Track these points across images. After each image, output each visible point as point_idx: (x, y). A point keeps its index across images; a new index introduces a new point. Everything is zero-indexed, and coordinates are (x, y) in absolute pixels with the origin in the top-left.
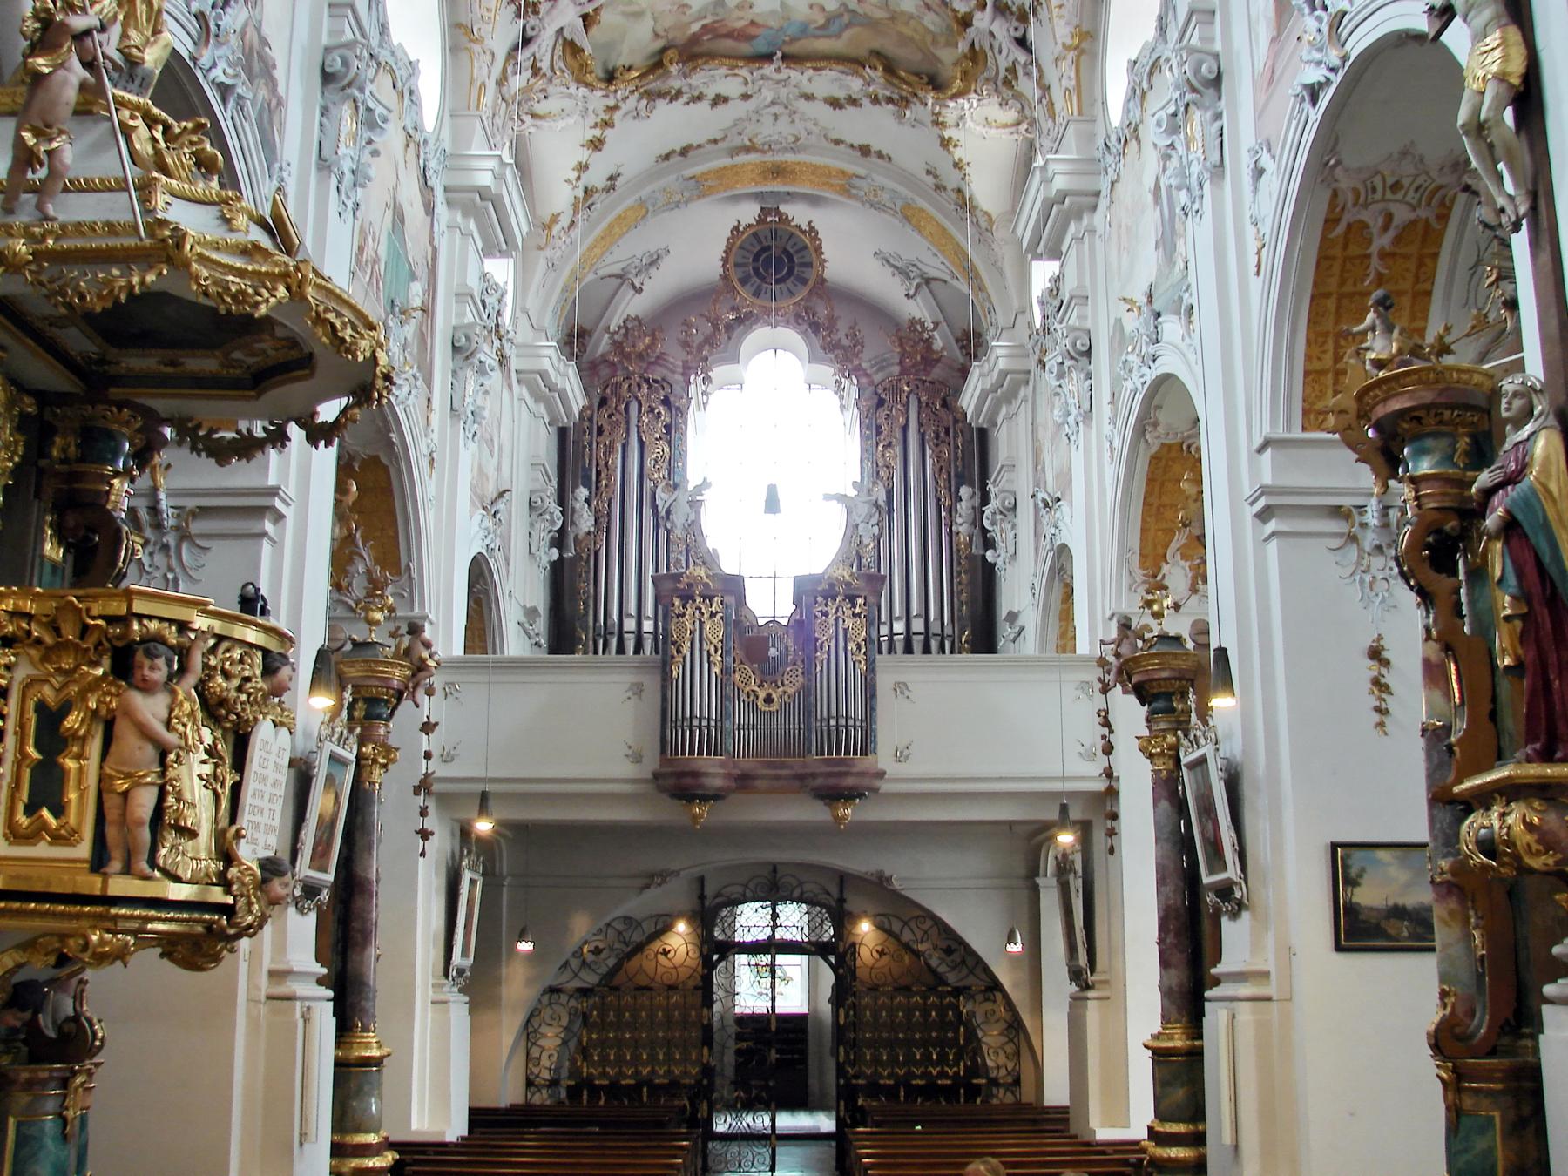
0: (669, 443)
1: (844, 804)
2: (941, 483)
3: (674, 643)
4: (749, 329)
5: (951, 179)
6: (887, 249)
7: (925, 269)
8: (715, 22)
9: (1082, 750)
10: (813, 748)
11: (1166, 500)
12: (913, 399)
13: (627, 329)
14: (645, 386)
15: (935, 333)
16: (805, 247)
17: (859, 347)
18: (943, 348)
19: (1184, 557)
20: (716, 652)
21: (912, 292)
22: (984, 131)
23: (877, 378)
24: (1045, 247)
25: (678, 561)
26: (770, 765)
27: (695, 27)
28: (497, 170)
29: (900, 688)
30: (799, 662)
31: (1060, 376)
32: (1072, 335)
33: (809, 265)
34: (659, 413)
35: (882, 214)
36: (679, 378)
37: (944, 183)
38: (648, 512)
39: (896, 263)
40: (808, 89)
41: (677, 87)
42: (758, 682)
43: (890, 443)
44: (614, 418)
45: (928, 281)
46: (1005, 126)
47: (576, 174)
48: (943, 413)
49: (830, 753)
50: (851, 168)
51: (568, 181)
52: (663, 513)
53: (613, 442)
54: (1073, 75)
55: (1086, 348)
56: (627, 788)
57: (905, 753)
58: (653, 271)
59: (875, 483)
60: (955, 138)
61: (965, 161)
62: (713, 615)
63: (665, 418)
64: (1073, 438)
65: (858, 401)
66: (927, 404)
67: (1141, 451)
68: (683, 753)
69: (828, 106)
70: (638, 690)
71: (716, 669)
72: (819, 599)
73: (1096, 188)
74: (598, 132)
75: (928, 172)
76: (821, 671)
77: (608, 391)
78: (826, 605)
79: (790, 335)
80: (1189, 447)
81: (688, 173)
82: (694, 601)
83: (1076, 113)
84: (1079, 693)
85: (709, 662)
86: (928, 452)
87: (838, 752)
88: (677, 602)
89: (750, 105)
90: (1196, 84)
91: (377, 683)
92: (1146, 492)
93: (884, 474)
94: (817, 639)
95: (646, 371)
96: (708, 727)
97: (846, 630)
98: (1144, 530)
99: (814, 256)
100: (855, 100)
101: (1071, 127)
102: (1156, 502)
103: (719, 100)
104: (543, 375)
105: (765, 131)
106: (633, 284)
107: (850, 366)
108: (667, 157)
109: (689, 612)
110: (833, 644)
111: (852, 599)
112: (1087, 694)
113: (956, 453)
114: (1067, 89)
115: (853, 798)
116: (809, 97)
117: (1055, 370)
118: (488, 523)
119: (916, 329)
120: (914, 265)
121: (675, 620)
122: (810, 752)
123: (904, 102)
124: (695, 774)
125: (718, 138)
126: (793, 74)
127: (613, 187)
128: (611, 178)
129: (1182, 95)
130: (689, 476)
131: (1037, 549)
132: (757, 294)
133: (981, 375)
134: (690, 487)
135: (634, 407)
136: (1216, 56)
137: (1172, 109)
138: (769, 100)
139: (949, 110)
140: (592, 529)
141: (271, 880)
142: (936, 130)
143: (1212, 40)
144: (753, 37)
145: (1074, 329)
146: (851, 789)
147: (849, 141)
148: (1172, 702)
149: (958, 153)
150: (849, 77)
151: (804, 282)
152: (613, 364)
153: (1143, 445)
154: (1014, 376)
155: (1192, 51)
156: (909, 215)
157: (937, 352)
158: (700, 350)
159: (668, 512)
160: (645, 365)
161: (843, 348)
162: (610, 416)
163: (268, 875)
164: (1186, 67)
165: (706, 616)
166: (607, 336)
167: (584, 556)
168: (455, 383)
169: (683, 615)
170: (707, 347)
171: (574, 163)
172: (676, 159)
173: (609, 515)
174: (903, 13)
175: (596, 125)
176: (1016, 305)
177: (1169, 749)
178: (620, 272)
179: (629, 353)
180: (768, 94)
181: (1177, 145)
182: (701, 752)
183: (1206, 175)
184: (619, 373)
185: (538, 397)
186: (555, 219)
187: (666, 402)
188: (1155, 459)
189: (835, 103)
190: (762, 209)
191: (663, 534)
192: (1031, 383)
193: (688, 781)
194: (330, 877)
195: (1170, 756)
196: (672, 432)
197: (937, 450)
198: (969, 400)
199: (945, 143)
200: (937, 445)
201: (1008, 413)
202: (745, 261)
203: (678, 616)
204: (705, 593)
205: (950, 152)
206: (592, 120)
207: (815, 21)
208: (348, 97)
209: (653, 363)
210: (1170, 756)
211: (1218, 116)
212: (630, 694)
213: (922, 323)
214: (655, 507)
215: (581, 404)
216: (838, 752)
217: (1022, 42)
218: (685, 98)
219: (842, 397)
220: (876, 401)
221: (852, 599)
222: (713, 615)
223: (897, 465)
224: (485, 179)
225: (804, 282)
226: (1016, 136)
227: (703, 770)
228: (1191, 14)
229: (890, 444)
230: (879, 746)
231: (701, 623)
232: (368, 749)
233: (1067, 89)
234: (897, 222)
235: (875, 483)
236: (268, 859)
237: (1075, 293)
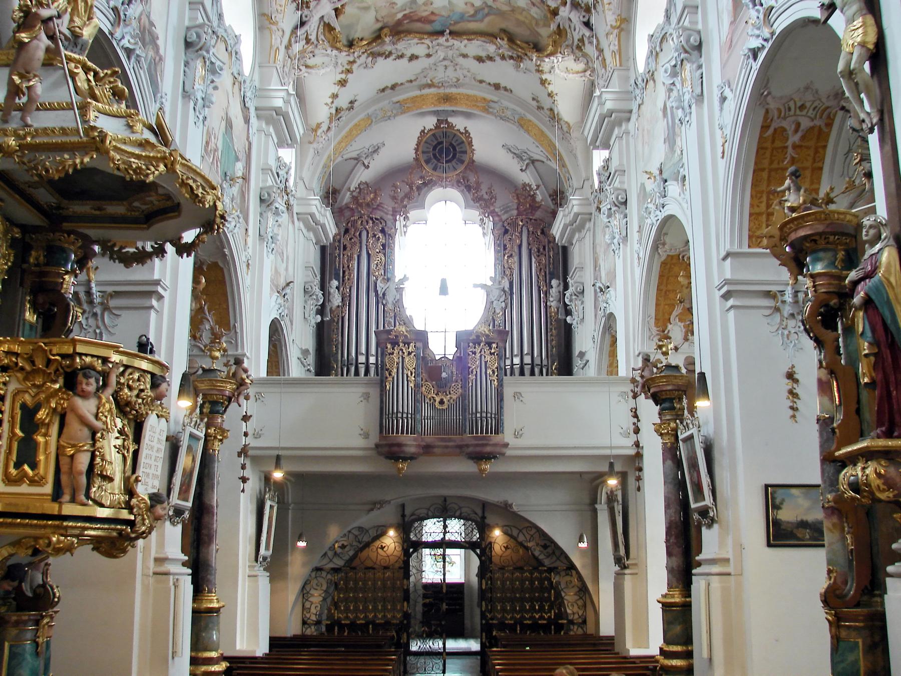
0: (385, 255)
1: (485, 462)
2: (541, 278)
3: (387, 370)
4: (430, 189)
5: (546, 103)
6: (510, 143)
7: (532, 155)
8: (411, 13)
9: (622, 431)
10: (467, 430)
11: (670, 287)
12: (525, 229)
13: (360, 189)
14: (371, 222)
15: (537, 191)
16: (463, 142)
17: (494, 200)
18: (542, 200)
19: (680, 320)
20: (411, 375)
21: (524, 168)
22: (565, 75)
23: (504, 217)
24: (601, 142)
25: (390, 323)
26: (442, 440)
27: (400, 16)
28: (285, 97)
29: (517, 395)
30: (459, 381)
31: (609, 216)
32: (616, 193)
33: (465, 152)
34: (379, 237)
35: (507, 123)
36: (390, 217)
37: (543, 105)
38: (372, 294)
39: (515, 151)
40: (465, 51)
41: (389, 50)
42: (436, 392)
43: (511, 255)
44: (353, 241)
45: (533, 162)
46: (578, 72)
47: (331, 100)
48: (542, 237)
49: (477, 433)
50: (489, 97)
51: (326, 104)
52: (381, 295)
53: (352, 254)
54: (616, 43)
55: (624, 200)
56: (360, 453)
57: (520, 433)
58: (375, 156)
59: (503, 278)
60: (549, 79)
61: (554, 93)
62: (409, 353)
63: (382, 240)
64: (616, 252)
65: (493, 231)
66: (533, 233)
67: (656, 259)
68: (393, 433)
69: (476, 61)
70: (366, 396)
71: (412, 385)
72: (471, 344)
73: (630, 108)
74: (343, 76)
75: (534, 99)
76: (472, 386)
77: (350, 225)
78: (475, 348)
79: (454, 193)
80: (683, 257)
81: (395, 99)
82: (399, 346)
83: (618, 65)
84: (620, 398)
85: (407, 381)
86: (533, 260)
87: (482, 432)
88: (389, 346)
89: (431, 60)
90: (687, 49)
91: (217, 393)
92: (659, 283)
93: (508, 272)
94: (469, 368)
95: (371, 213)
96: (407, 418)
97: (486, 362)
98: (657, 305)
99: (468, 147)
100: (491, 57)
101: (616, 73)
102: (664, 289)
103: (413, 57)
104: (312, 215)
105: (440, 75)
106: (364, 164)
107: (488, 211)
108: (383, 90)
109: (396, 352)
110: (478, 370)
111: (489, 344)
112: (625, 399)
113: (549, 261)
114: (613, 51)
115: (490, 459)
116: (465, 56)
117: (606, 213)
118: (281, 300)
119: (526, 189)
120: (525, 152)
121: (388, 356)
122: (465, 432)
123: (519, 59)
124: (400, 445)
125: (413, 79)
126: (456, 42)
127: (352, 108)
128: (351, 102)
129: (679, 55)
130: (396, 274)
131: (596, 316)
132: (435, 169)
133: (564, 216)
134: (397, 280)
135: (364, 234)
136: (699, 32)
137: (673, 63)
138: (442, 57)
139: (545, 63)
140: (340, 304)
141: (156, 506)
142: (538, 75)
143: (697, 23)
144: (433, 21)
145: (617, 189)
146: (489, 453)
147: (488, 81)
148: (673, 403)
149: (550, 88)
150: (488, 45)
151: (462, 162)
152: (352, 209)
153: (657, 256)
154: (583, 216)
155: (685, 29)
156: (523, 124)
157: (539, 203)
158: (402, 201)
159: (384, 294)
160: (370, 210)
161: (485, 200)
162: (351, 239)
163: (154, 503)
164: (682, 38)
165: (406, 354)
166: (349, 193)
167: (336, 319)
168: (262, 220)
169: (393, 354)
170: (406, 200)
171: (330, 94)
172: (388, 91)
173: (350, 296)
174: (519, 7)
175: (342, 72)
176: (584, 175)
177: (672, 431)
178: (356, 156)
179: (362, 203)
180: (441, 54)
181: (677, 84)
182: (403, 432)
183: (693, 101)
184: (356, 214)
185: (309, 228)
186: (319, 126)
187: (383, 231)
188: (664, 264)
189: (480, 59)
190: (438, 120)
191: (381, 307)
192: (592, 220)
193: (395, 449)
194: (189, 504)
195: (672, 435)
196: (386, 248)
197: (538, 259)
198: (557, 230)
199: (543, 82)
200: (538, 256)
201: (579, 237)
202: (428, 150)
203: (390, 354)
204: (405, 341)
205: (546, 88)
206: (340, 69)
207: (469, 12)
208: (200, 56)
209: (375, 209)
210: (672, 435)
211: (700, 67)
212: (362, 399)
213: (530, 186)
214: (376, 291)
215: (334, 232)
216: (482, 432)
217: (587, 24)
218: (393, 57)
219: (484, 228)
220: (503, 230)
221: (489, 344)
222: (409, 353)
223: (516, 267)
224: (279, 103)
225: (462, 162)
226: (584, 78)
227: (404, 443)
228: (684, 8)
229: (511, 255)
230: (505, 429)
231: (403, 358)
232: (211, 431)
233: (613, 51)
234: (515, 127)
235: (503, 278)
236: (154, 494)
237: (618, 168)
